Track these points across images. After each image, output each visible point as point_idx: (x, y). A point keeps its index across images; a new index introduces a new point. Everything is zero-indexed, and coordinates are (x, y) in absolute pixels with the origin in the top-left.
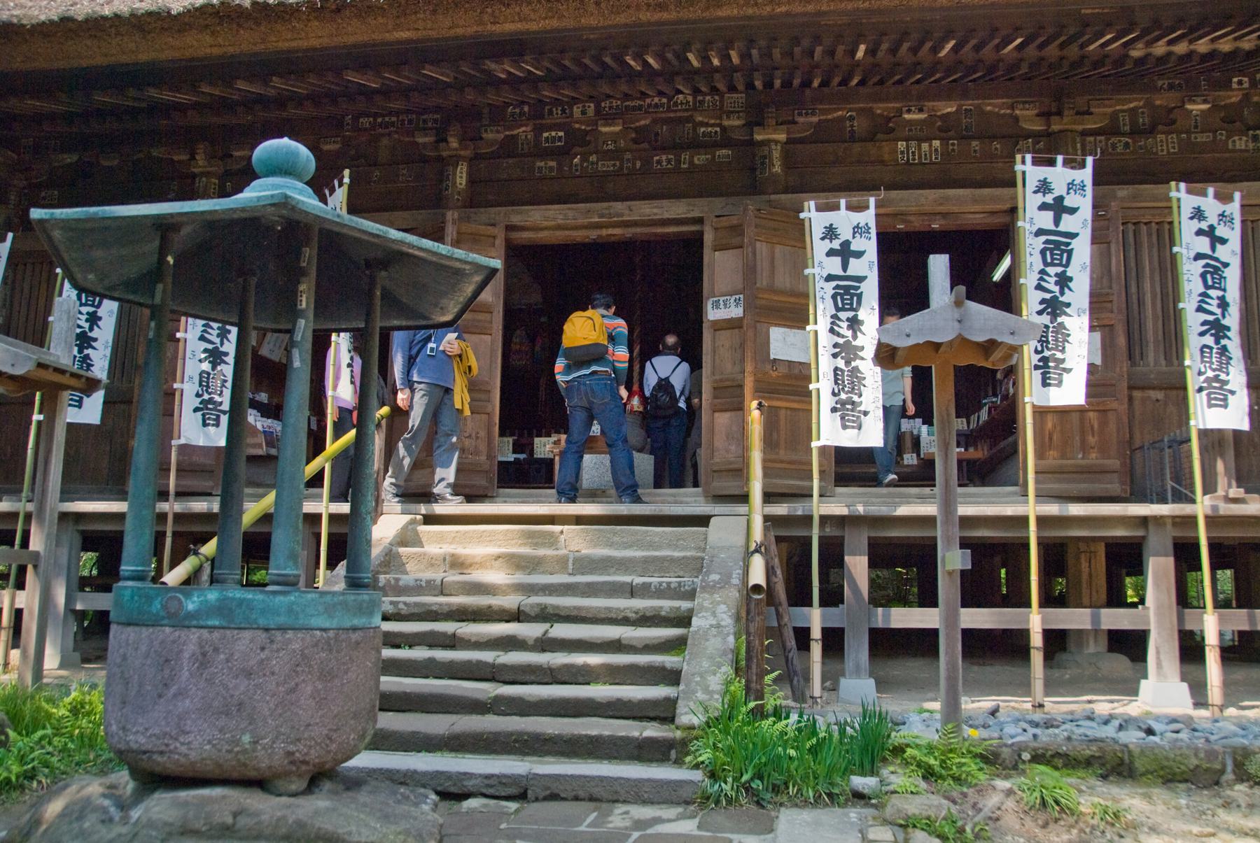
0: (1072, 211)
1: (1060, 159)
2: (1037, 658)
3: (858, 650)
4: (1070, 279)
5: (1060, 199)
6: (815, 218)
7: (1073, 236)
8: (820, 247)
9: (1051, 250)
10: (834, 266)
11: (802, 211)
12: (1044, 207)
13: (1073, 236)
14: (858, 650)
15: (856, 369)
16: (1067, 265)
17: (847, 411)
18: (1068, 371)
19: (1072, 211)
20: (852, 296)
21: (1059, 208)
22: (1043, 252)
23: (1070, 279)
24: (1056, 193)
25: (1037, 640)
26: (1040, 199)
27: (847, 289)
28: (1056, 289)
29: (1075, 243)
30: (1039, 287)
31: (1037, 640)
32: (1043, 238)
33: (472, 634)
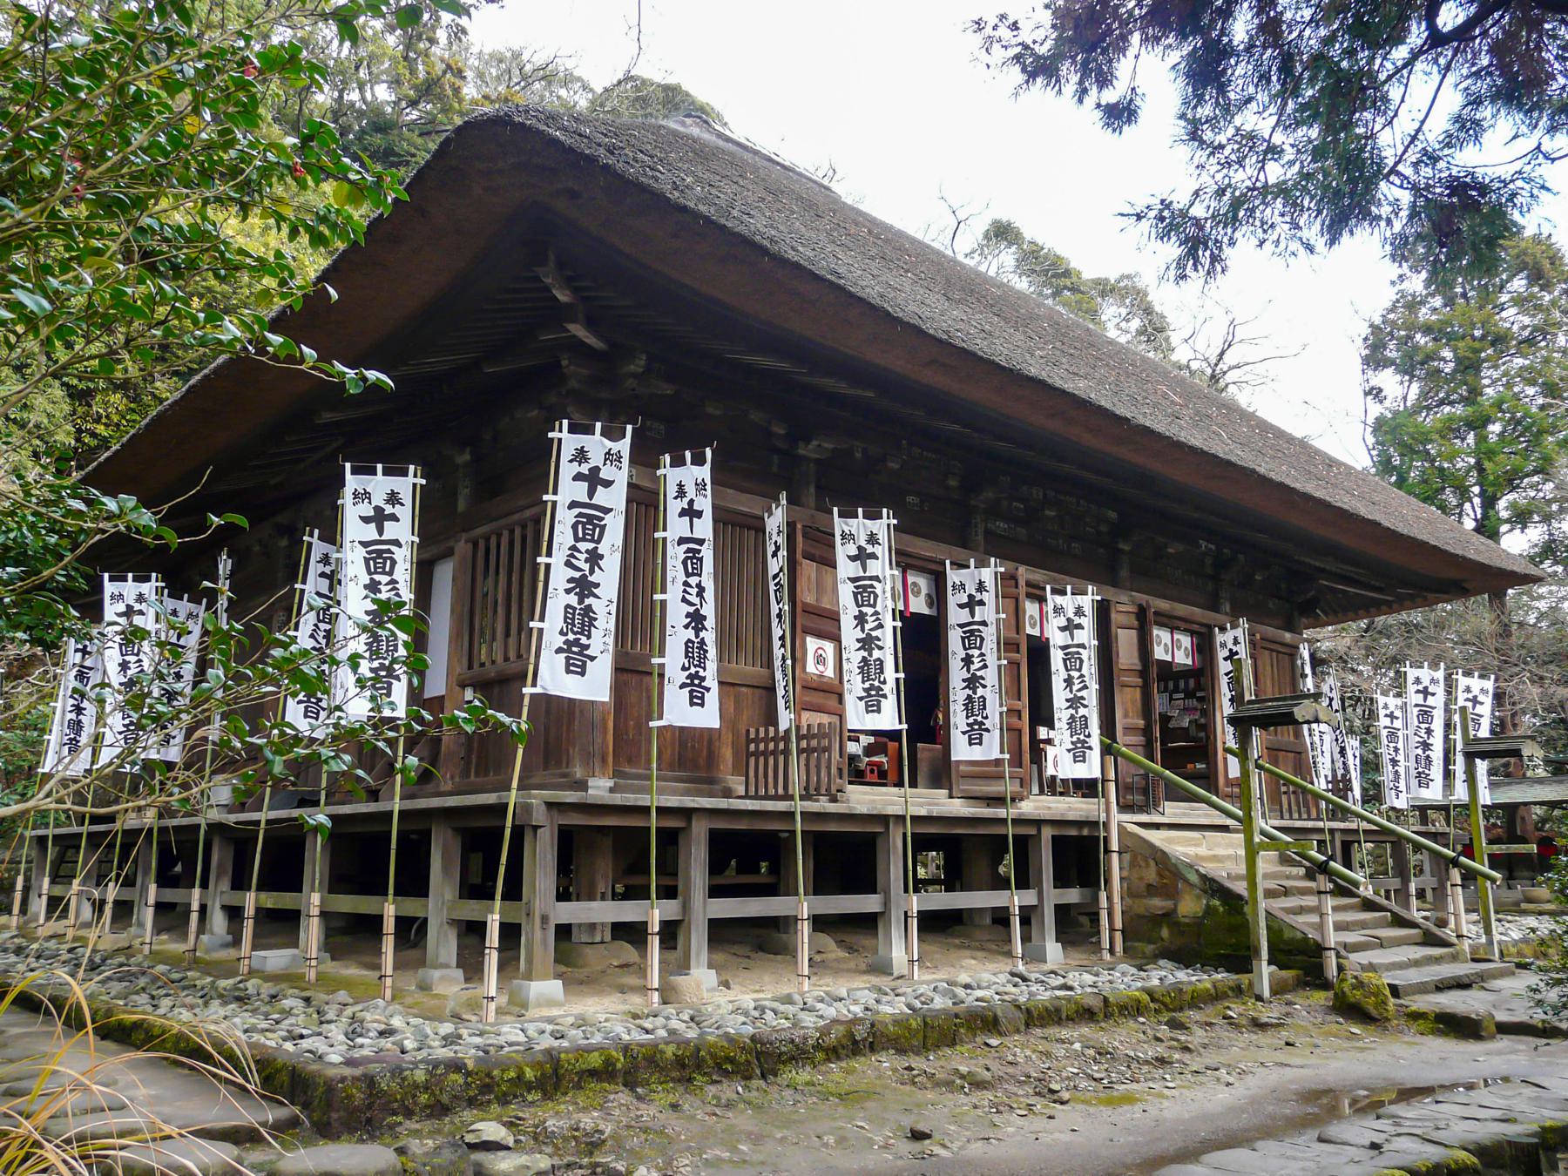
0: (608, 484)
1: (130, 575)
2: (388, 944)
3: (698, 937)
4: (601, 557)
5: (596, 470)
6: (566, 440)
7: (607, 511)
8: (568, 470)
9: (584, 524)
10: (580, 491)
11: (553, 430)
12: (578, 477)
13: (607, 511)
14: (698, 937)
15: (589, 608)
16: (598, 542)
17: (577, 659)
18: (592, 659)
19: (608, 484)
20: (595, 526)
21: (593, 480)
22: (575, 527)
23: (601, 557)
24: (592, 464)
25: (389, 926)
26: (575, 468)
27: (590, 518)
28: (586, 567)
29: (608, 519)
30: (312, 636)
31: (389, 926)
32: (577, 511)
33: (688, 879)
